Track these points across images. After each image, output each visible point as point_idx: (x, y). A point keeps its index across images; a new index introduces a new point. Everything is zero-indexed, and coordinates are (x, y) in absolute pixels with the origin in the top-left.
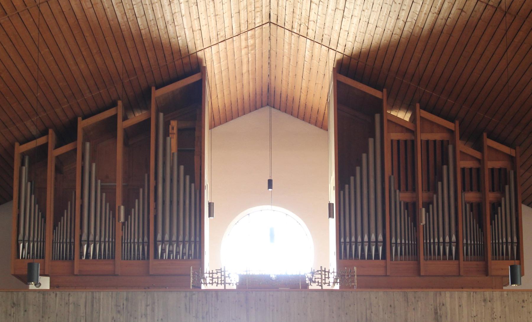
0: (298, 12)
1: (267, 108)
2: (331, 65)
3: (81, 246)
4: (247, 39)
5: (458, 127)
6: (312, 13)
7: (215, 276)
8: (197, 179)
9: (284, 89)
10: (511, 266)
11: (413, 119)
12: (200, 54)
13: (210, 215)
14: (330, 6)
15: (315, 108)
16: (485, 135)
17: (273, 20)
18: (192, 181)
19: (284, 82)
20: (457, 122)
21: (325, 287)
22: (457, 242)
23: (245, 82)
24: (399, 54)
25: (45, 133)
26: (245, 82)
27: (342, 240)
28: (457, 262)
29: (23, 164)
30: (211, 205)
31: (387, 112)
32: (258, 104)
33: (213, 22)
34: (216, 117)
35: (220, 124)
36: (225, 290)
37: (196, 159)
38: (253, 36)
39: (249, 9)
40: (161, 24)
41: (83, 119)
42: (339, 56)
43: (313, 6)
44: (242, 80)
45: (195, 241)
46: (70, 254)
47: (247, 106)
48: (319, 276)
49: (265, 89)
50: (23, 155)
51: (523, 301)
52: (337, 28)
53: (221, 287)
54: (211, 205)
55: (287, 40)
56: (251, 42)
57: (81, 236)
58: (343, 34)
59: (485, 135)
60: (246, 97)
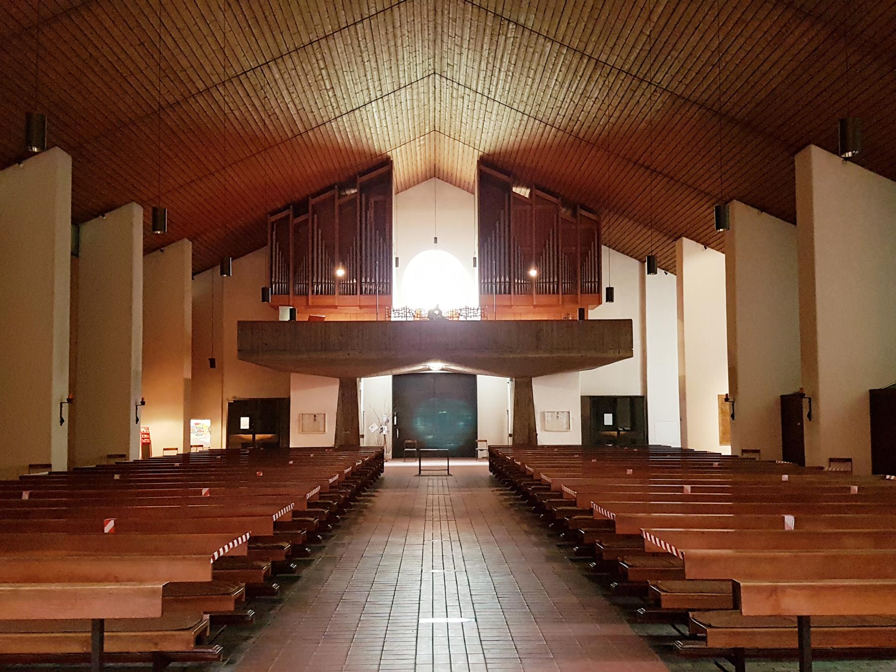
0: (453, 126)
1: (434, 179)
2: (476, 159)
3: (313, 286)
4: (420, 141)
5: (560, 201)
6: (462, 128)
7: (400, 312)
8: (388, 241)
9: (445, 168)
10: (579, 309)
11: (531, 194)
12: (389, 153)
13: (397, 265)
14: (473, 126)
15: (467, 181)
16: (578, 206)
17: (437, 129)
18: (384, 240)
19: (445, 165)
20: (560, 199)
21: (469, 319)
22: (558, 282)
23: (419, 165)
24: (519, 154)
25: (286, 207)
26: (419, 165)
27: (482, 281)
28: (557, 295)
29: (272, 231)
30: (397, 259)
31: (514, 189)
32: (428, 177)
33: (397, 135)
34: (399, 187)
35: (402, 191)
36: (406, 321)
37: (387, 225)
38: (424, 139)
39: (421, 125)
40: (364, 140)
41: (312, 198)
42: (481, 153)
43: (463, 124)
44: (416, 165)
45: (387, 283)
46: (306, 291)
47: (420, 179)
48: (465, 312)
49: (433, 168)
50: (273, 223)
51: (592, 327)
52: (478, 138)
53: (404, 319)
54: (397, 259)
55: (446, 141)
56: (422, 143)
57: (312, 279)
58: (483, 142)
59: (578, 206)
60: (420, 174)
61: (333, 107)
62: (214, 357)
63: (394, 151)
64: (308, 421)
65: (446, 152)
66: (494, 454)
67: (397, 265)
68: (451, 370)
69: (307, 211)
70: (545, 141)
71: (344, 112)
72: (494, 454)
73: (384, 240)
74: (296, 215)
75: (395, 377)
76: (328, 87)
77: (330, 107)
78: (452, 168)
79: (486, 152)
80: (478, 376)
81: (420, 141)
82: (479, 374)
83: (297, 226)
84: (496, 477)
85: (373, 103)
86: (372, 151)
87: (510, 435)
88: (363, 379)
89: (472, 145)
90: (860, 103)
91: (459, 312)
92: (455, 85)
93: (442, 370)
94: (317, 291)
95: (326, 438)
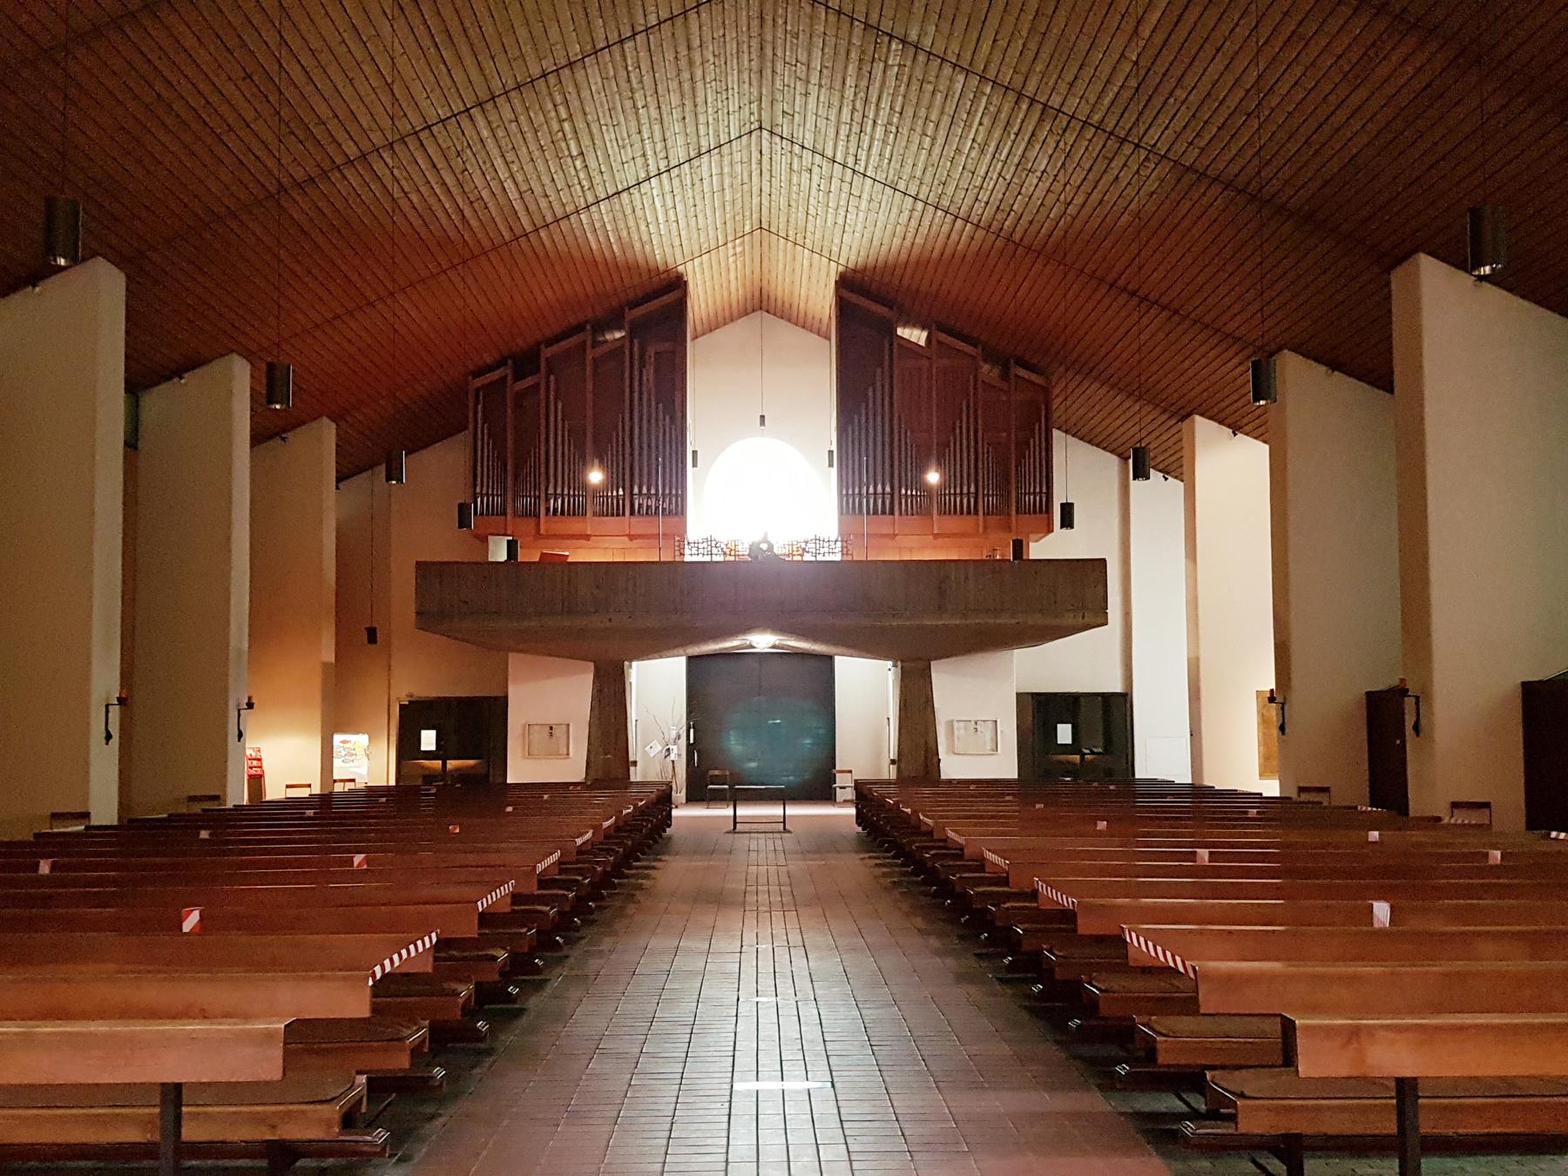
0: (792, 220)
1: (759, 313)
2: (833, 278)
3: (547, 500)
4: (734, 248)
5: (980, 352)
6: (809, 225)
7: (701, 546)
8: (679, 422)
9: (779, 294)
10: (1014, 541)
11: (929, 339)
12: (680, 269)
13: (695, 465)
14: (829, 220)
15: (817, 317)
16: (1012, 361)
17: (765, 226)
18: (672, 419)
19: (779, 288)
20: (980, 348)
21: (820, 558)
22: (976, 493)
23: (733, 289)
24: (909, 270)
25: (501, 363)
26: (733, 289)
27: (844, 492)
28: (975, 517)
29: (476, 404)
30: (695, 453)
31: (900, 331)
32: (750, 309)
33: (696, 236)
34: (699, 328)
35: (704, 334)
36: (711, 562)
37: (678, 394)
38: (743, 244)
39: (737, 218)
40: (637, 246)
41: (546, 347)
42: (841, 269)
43: (810, 217)
44: (729, 288)
45: (677, 495)
46: (535, 509)
47: (735, 313)
48: (813, 546)
49: (757, 294)
50: (478, 390)
51: (1036, 573)
52: (837, 241)
53: (707, 559)
54: (695, 453)
55: (781, 246)
56: (739, 249)
57: (547, 489)
58: (845, 249)
59: (1012, 361)
60: (734, 305)
61: (582, 187)
62: (374, 625)
63: (689, 265)
64: (539, 736)
65: (781, 266)
66: (864, 794)
67: (695, 465)
68: (789, 647)
69: (538, 370)
70: (953, 246)
71: (603, 196)
72: (864, 794)
73: (672, 419)
74: (519, 376)
75: (690, 659)
76: (575, 153)
77: (578, 187)
78: (792, 294)
79: (851, 265)
80: (836, 657)
81: (734, 248)
82: (838, 655)
83: (520, 396)
84: (869, 834)
85: (652, 180)
86: (651, 263)
87: (893, 762)
88: (634, 664)
89: (826, 253)
90: (1505, 181)
91: (803, 545)
92: (797, 148)
93: (774, 647)
94: (555, 510)
95: (571, 767)
